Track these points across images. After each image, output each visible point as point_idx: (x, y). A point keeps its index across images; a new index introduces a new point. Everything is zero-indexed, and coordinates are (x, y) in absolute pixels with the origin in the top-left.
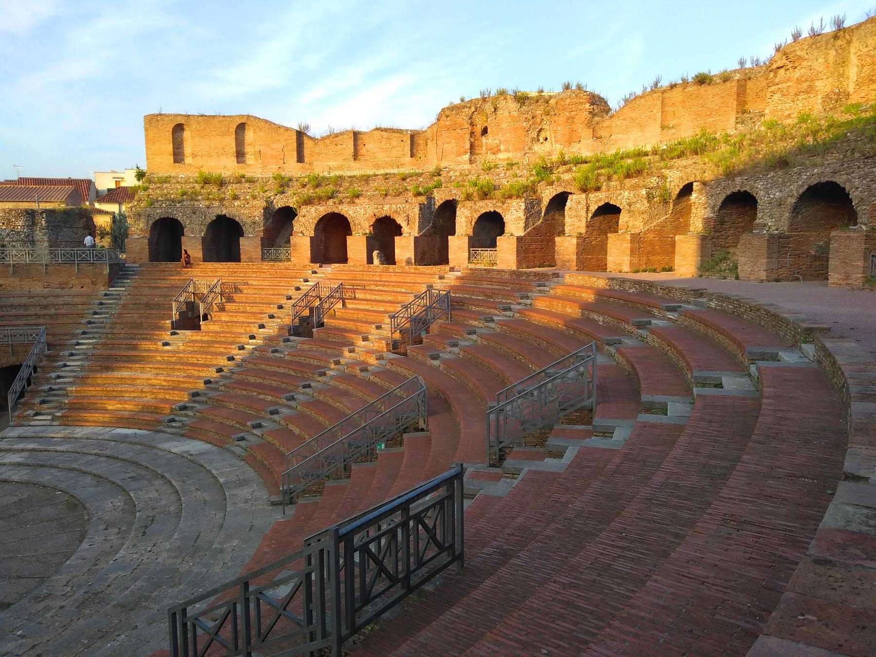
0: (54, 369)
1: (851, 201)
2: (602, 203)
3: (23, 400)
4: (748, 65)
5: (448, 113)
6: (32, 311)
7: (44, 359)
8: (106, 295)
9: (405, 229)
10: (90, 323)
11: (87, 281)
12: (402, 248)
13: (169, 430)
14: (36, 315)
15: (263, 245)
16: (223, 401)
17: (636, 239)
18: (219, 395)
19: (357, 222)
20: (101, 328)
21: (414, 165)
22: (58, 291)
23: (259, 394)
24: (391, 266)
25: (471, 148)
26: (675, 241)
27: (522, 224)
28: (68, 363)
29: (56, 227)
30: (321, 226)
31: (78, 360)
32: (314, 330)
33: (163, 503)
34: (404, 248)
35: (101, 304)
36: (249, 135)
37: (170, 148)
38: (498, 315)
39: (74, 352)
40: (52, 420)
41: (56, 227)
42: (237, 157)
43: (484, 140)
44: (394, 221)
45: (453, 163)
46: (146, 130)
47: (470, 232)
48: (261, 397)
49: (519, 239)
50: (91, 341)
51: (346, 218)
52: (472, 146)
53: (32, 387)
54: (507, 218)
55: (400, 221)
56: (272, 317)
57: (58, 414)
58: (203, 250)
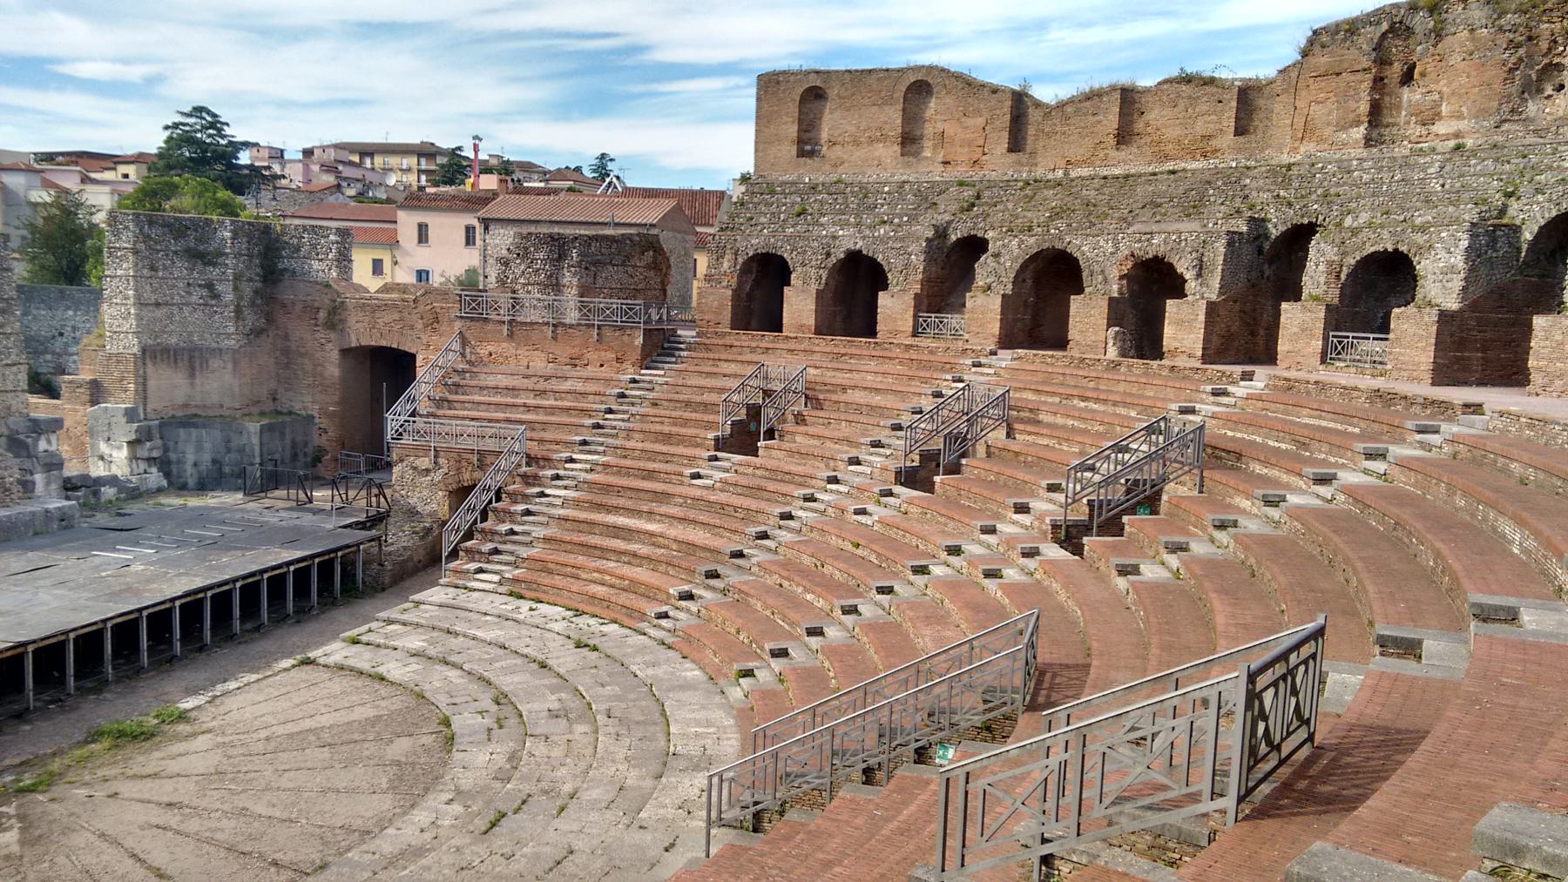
0: (526, 498)
3: (469, 544)
5: (1324, 39)
7: (518, 479)
8: (634, 381)
9: (1191, 286)
10: (598, 426)
12: (1180, 323)
13: (652, 632)
14: (525, 405)
15: (917, 309)
16: (747, 594)
17: (1445, 317)
18: (745, 583)
19: (1097, 268)
20: (612, 436)
21: (1239, 150)
23: (806, 590)
24: (1155, 364)
25: (1371, 114)
27: (1457, 283)
28: (548, 491)
29: (595, 264)
30: (1028, 274)
32: (937, 479)
34: (1184, 325)
35: (622, 396)
37: (793, 130)
38: (1304, 492)
39: (561, 472)
41: (595, 264)
42: (903, 144)
43: (1406, 94)
45: (1320, 144)
46: (759, 99)
47: (1334, 296)
48: (809, 597)
49: (1445, 317)
50: (589, 457)
51: (1076, 260)
52: (1376, 111)
53: (487, 525)
54: (1423, 266)
55: (1184, 267)
56: (877, 444)
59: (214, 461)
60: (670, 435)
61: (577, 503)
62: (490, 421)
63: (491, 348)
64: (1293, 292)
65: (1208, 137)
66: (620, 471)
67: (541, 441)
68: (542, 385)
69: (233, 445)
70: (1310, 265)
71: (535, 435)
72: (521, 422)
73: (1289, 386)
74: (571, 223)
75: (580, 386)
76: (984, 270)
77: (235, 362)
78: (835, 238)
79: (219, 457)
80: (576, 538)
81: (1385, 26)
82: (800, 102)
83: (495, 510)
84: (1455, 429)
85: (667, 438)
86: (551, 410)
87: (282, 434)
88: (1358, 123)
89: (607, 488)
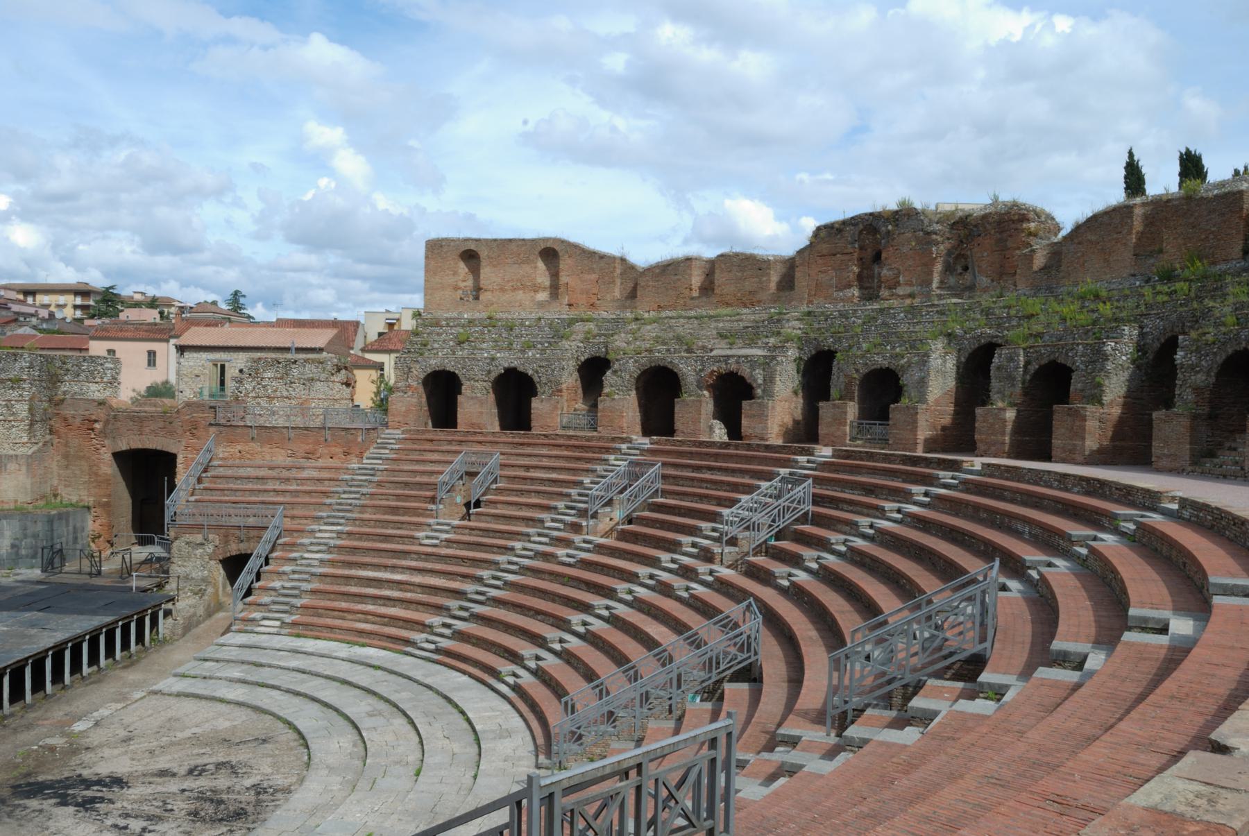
2: (1044, 361)
6: (270, 486)
11: (339, 450)
14: (274, 491)
26: (1151, 420)
28: (306, 555)
33: (401, 750)
36: (565, 264)
50: (334, 528)
57: (288, 621)
59: (13, 546)
60: (397, 508)
61: (332, 563)
62: (248, 503)
63: (239, 447)
64: (1168, 403)
66: (361, 536)
67: (293, 517)
68: (285, 474)
69: (29, 532)
70: (834, 377)
71: (289, 513)
72: (281, 504)
75: (315, 474)
77: (28, 465)
78: (493, 359)
79: (17, 542)
80: (336, 588)
81: (861, 226)
86: (295, 493)
87: (67, 522)
88: (849, 286)
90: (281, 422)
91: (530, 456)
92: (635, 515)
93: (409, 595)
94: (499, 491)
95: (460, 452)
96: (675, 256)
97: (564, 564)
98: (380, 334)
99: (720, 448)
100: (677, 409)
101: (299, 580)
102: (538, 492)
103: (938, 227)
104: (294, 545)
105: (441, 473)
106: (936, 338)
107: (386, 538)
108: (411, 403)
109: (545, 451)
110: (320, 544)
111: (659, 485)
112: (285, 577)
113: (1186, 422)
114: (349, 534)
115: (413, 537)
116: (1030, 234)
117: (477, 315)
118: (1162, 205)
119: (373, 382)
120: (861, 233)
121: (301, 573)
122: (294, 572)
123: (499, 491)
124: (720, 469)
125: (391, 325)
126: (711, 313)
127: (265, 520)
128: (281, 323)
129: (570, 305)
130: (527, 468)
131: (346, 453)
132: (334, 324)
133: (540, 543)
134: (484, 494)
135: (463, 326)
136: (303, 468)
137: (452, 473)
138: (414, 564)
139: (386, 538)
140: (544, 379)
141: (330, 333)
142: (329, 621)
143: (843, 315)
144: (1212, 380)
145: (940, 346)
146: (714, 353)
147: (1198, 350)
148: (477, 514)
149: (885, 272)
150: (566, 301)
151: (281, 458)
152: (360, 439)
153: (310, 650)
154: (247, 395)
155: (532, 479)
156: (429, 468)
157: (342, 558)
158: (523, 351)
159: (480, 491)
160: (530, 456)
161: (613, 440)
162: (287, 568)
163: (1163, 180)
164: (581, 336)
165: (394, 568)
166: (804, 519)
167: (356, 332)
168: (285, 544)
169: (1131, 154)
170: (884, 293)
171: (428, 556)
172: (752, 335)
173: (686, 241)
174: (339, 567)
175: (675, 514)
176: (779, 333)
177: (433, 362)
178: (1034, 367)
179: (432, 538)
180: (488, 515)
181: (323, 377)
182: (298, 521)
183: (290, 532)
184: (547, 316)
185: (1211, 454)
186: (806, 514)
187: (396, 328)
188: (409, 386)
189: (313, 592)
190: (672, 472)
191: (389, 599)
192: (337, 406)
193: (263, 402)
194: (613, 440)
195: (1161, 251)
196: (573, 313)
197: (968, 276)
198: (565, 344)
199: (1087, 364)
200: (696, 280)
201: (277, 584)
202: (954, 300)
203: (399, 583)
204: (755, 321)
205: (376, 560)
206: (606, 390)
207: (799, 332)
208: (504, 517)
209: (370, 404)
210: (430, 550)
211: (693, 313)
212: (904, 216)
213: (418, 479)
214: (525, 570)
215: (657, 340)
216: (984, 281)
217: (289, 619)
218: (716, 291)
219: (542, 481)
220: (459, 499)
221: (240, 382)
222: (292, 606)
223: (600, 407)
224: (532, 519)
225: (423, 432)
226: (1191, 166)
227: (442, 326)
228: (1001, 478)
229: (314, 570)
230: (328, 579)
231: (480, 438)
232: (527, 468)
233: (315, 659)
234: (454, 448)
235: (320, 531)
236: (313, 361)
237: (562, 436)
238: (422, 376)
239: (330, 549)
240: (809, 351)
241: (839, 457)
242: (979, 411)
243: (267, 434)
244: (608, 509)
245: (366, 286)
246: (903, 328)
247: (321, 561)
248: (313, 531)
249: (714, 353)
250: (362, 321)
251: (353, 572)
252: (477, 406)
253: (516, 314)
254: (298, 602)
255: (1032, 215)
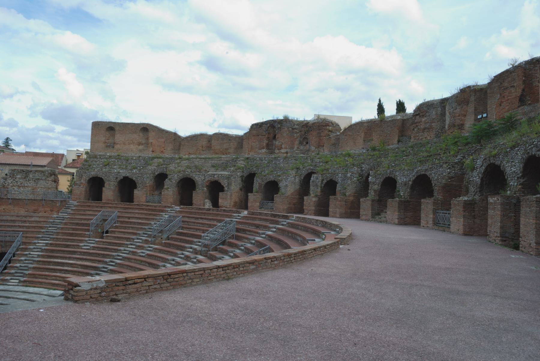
1: (432, 184)
2: (328, 179)
3: (6, 271)
4: (410, 109)
14: (19, 226)
22: (32, 214)
28: (31, 253)
31: (37, 252)
34: (226, 200)
40: (19, 283)
44: (220, 184)
50: (45, 242)
54: (281, 185)
55: (224, 183)
58: (133, 194)
60: (73, 234)
61: (43, 256)
62: (7, 231)
63: (4, 207)
65: (226, 149)
66: (56, 245)
67: (26, 237)
68: (24, 219)
70: (255, 184)
71: (25, 235)
72: (21, 231)
73: (253, 214)
74: (20, 165)
75: (37, 219)
76: (167, 182)
78: (119, 173)
81: (269, 125)
82: (105, 131)
83: (13, 260)
84: (289, 221)
85: (71, 235)
86: (28, 227)
88: (263, 148)
89: (52, 251)
90: (24, 197)
91: (130, 213)
92: (170, 236)
93: (75, 269)
94: (116, 227)
95: (100, 211)
96: (196, 133)
97: (141, 256)
98: (73, 160)
99: (207, 210)
100: (194, 195)
101: (28, 263)
102: (132, 228)
103: (296, 127)
104: (26, 249)
105: (92, 219)
106: (293, 169)
107: (67, 246)
108: (81, 190)
109: (137, 211)
110: (38, 248)
111: (181, 224)
112: (22, 262)
113: (370, 202)
114: (51, 244)
115: (78, 246)
116: (329, 131)
117: (113, 154)
118: (392, 120)
119: (68, 181)
120: (268, 127)
121: (29, 260)
122: (26, 260)
123: (116, 227)
124: (205, 219)
125: (79, 156)
126: (210, 157)
127: (14, 238)
128: (28, 154)
129: (153, 151)
130: (129, 218)
131: (52, 211)
132: (53, 155)
133: (132, 248)
134: (110, 228)
135: (107, 158)
136: (32, 217)
137: (97, 219)
138: (78, 256)
139: (67, 246)
140: (140, 182)
141: (49, 159)
142: (40, 280)
143: (261, 159)
144: (380, 187)
145: (294, 172)
146: (209, 173)
147: (375, 177)
148: (107, 236)
149: (277, 143)
150: (151, 150)
151: (22, 212)
152: (58, 205)
153: (31, 291)
154: (8, 185)
155: (131, 222)
156: (87, 217)
157: (47, 254)
158: (131, 170)
159: (108, 227)
160: (130, 213)
161: (165, 207)
162: (23, 258)
163: (390, 111)
164: (156, 164)
165: (70, 258)
166: (232, 237)
167: (62, 159)
168: (23, 248)
169: (380, 101)
170: (277, 151)
171: (85, 253)
172: (225, 167)
173: (219, 126)
174: (46, 258)
175: (186, 236)
176: (235, 166)
177: (92, 173)
178: (325, 181)
179: (87, 246)
180: (111, 236)
181: (44, 178)
182: (28, 239)
183: (24, 243)
184: (143, 155)
185: (379, 214)
186: (233, 235)
187: (81, 157)
188: (82, 183)
189: (34, 268)
190: (187, 219)
191: (66, 270)
192: (50, 191)
193: (16, 188)
194: (165, 207)
195: (372, 140)
196: (154, 155)
197: (308, 146)
198: (149, 167)
199: (342, 180)
200: (204, 143)
201: (18, 265)
202: (302, 155)
203: (71, 264)
204: (227, 161)
205: (62, 255)
206: (165, 187)
207: (243, 165)
208: (118, 237)
209: (67, 190)
210: (85, 251)
211: (203, 157)
212: (286, 121)
213: (83, 222)
214: (124, 259)
215: (188, 167)
216: (313, 148)
217: (22, 279)
218: (213, 148)
219: (135, 223)
220: (99, 230)
221: (6, 179)
222: (24, 274)
223: (163, 193)
224: (129, 238)
225: (86, 202)
226: (401, 106)
227: (97, 158)
228: (301, 222)
229: (34, 259)
230: (41, 263)
231: (110, 205)
232: (129, 218)
233: (33, 295)
234: (99, 209)
235: (38, 243)
236: (39, 171)
237: (144, 205)
238: (87, 179)
239: (42, 251)
240: (246, 174)
241: (250, 214)
242: (305, 198)
243: (16, 202)
244: (160, 234)
245: (75, 139)
246: (282, 165)
247: (38, 255)
248: (35, 243)
249: (209, 173)
250: (66, 154)
251: (52, 260)
252: (109, 192)
253: (130, 154)
254: (27, 272)
255: (330, 124)
